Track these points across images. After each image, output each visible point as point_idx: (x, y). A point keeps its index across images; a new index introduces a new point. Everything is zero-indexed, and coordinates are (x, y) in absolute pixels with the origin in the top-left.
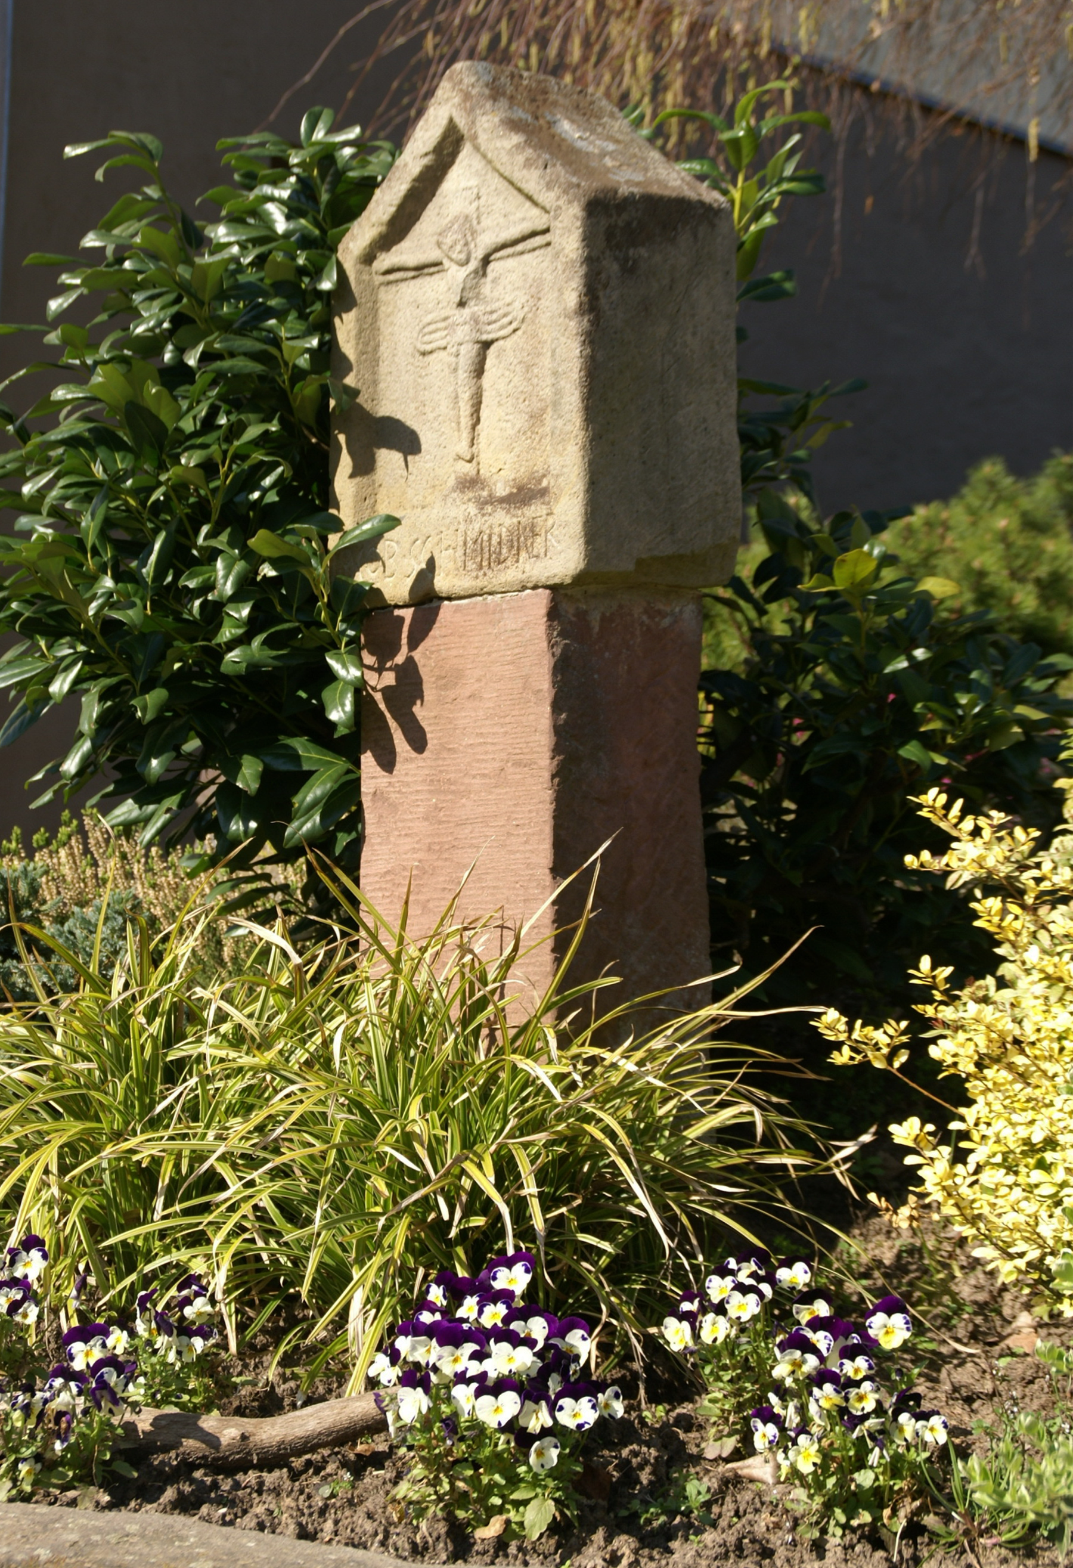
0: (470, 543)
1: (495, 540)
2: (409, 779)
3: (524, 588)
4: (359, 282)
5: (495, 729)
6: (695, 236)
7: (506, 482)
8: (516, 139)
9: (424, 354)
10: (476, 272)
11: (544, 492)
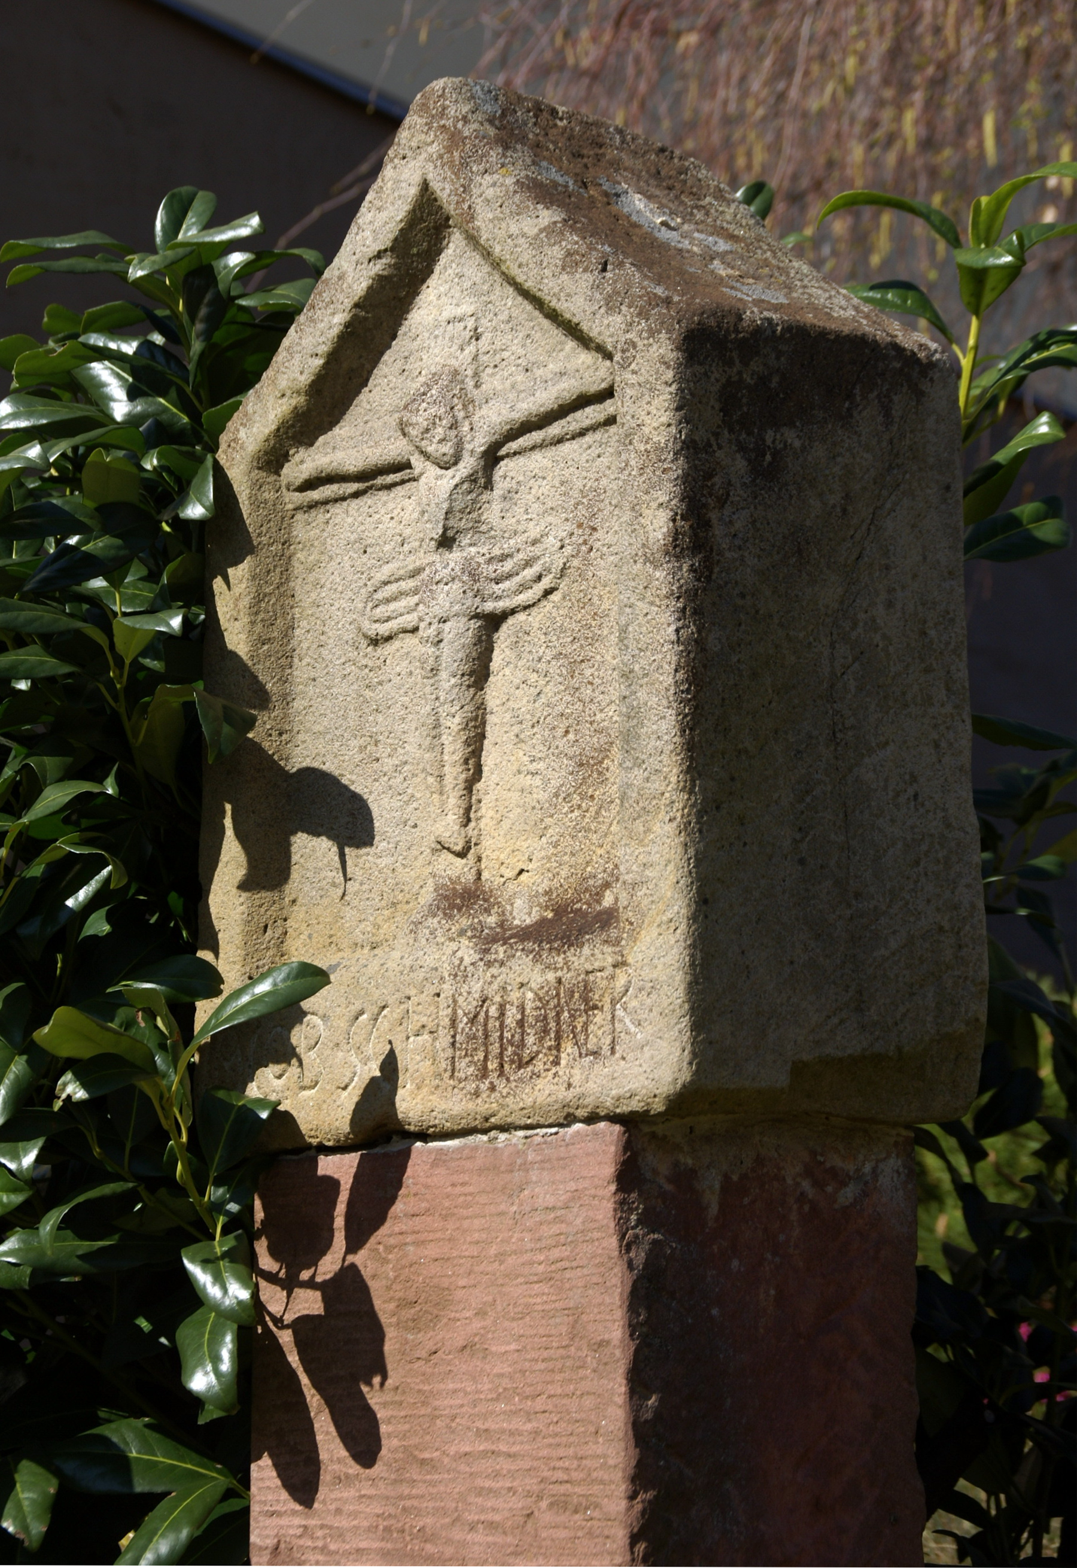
0: (463, 1023)
1: (512, 1015)
2: (343, 1523)
3: (570, 1119)
4: (257, 504)
5: (517, 1423)
6: (887, 414)
7: (533, 897)
8: (547, 216)
9: (375, 642)
10: (472, 479)
11: (607, 919)
